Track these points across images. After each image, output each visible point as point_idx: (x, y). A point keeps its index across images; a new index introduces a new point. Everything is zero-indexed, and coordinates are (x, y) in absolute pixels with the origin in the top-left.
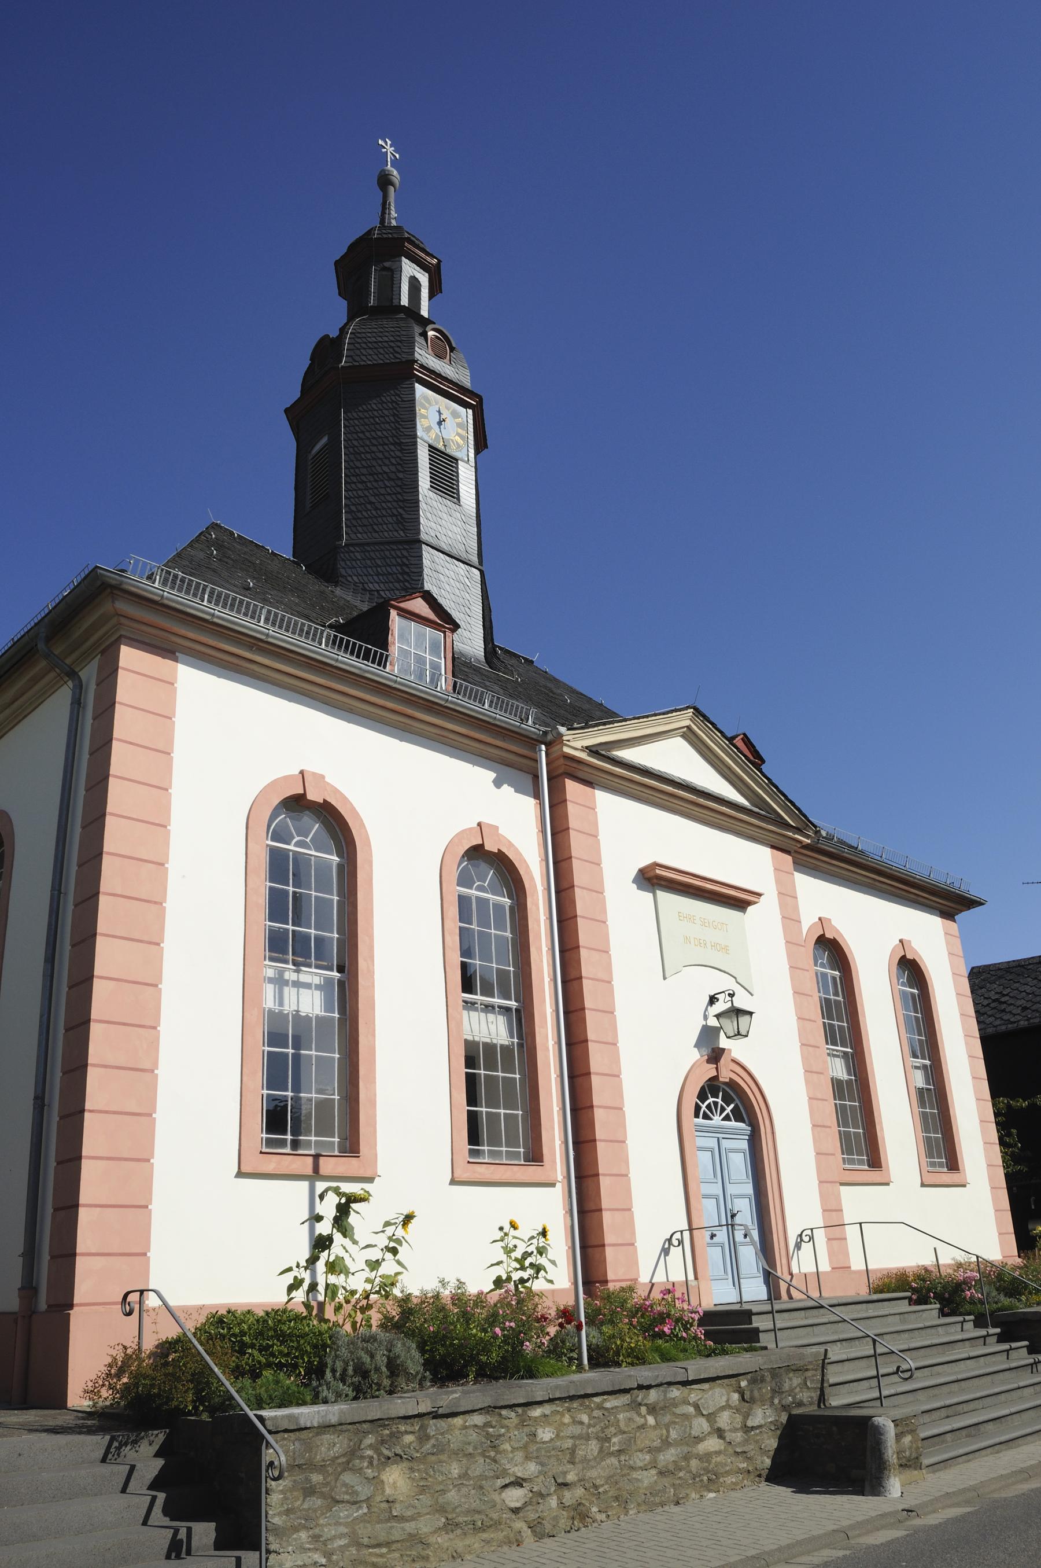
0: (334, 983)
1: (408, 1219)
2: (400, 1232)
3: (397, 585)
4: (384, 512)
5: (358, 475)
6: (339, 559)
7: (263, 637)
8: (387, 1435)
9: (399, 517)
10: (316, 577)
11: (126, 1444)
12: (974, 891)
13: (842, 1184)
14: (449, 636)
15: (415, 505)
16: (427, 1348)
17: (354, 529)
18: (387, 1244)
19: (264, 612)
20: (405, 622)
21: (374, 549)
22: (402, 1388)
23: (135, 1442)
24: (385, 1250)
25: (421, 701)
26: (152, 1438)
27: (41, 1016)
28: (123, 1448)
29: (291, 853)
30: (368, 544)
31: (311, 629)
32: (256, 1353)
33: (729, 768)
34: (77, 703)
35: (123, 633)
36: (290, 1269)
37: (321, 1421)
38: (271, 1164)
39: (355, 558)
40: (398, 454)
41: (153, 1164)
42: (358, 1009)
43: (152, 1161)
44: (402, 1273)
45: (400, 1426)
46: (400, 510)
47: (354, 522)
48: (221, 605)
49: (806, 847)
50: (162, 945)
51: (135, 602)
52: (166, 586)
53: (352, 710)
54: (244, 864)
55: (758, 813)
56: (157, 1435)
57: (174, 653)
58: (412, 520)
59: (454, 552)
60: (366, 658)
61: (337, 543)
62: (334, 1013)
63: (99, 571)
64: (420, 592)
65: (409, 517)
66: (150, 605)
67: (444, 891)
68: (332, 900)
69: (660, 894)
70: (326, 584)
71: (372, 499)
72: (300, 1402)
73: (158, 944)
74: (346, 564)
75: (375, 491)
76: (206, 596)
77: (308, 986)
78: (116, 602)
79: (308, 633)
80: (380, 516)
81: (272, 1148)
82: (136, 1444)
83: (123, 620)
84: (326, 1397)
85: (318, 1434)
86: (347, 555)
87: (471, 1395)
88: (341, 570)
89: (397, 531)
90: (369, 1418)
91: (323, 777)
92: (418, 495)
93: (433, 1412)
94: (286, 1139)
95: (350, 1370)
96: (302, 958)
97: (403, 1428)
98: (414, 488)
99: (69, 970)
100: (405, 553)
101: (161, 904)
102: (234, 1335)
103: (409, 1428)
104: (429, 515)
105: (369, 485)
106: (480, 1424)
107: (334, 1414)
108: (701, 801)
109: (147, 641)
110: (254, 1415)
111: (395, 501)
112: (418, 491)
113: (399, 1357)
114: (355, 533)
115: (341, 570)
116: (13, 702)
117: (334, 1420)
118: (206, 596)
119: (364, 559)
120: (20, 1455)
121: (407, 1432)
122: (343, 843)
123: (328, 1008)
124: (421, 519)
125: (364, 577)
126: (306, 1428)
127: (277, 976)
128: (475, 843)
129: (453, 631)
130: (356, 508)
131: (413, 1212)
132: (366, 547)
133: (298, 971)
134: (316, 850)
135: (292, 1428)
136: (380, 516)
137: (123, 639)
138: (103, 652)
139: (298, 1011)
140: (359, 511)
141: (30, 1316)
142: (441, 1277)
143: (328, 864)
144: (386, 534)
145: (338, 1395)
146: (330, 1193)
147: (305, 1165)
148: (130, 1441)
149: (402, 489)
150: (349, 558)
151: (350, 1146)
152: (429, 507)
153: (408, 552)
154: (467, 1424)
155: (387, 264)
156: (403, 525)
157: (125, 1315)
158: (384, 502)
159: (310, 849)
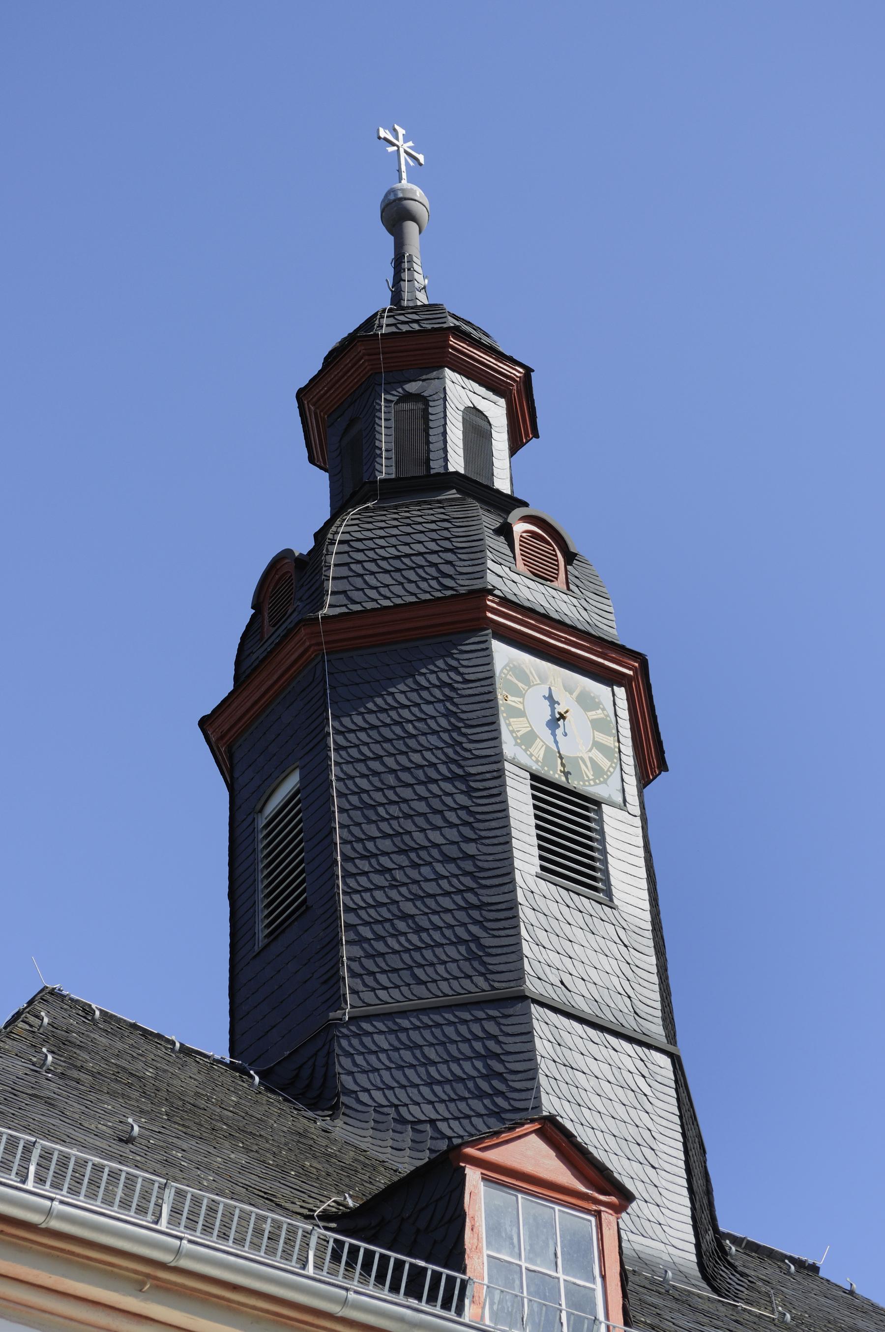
4: (437, 936)
5: (375, 855)
6: (337, 1050)
9: (473, 946)
10: (286, 1100)
14: (609, 1223)
17: (369, 980)
19: (169, 1196)
20: (501, 1196)
21: (418, 1023)
30: (403, 1013)
39: (374, 1048)
40: (463, 800)
46: (474, 929)
47: (369, 964)
52: (78, 1193)
58: (505, 950)
59: (607, 1017)
60: (414, 1291)
61: (332, 1015)
70: (310, 1114)
75: (415, 888)
76: (32, 1169)
80: (428, 946)
86: (355, 1042)
88: (343, 1077)
89: (469, 977)
92: (514, 891)
104: (542, 936)
105: (398, 875)
111: (461, 908)
114: (373, 990)
115: (343, 1077)
118: (32, 1169)
119: (397, 1050)
125: (397, 1090)
129: (619, 1209)
136: (428, 946)
144: (444, 985)
149: (475, 879)
153: (499, 1024)
155: (412, 387)
156: (484, 964)
158: (435, 912)
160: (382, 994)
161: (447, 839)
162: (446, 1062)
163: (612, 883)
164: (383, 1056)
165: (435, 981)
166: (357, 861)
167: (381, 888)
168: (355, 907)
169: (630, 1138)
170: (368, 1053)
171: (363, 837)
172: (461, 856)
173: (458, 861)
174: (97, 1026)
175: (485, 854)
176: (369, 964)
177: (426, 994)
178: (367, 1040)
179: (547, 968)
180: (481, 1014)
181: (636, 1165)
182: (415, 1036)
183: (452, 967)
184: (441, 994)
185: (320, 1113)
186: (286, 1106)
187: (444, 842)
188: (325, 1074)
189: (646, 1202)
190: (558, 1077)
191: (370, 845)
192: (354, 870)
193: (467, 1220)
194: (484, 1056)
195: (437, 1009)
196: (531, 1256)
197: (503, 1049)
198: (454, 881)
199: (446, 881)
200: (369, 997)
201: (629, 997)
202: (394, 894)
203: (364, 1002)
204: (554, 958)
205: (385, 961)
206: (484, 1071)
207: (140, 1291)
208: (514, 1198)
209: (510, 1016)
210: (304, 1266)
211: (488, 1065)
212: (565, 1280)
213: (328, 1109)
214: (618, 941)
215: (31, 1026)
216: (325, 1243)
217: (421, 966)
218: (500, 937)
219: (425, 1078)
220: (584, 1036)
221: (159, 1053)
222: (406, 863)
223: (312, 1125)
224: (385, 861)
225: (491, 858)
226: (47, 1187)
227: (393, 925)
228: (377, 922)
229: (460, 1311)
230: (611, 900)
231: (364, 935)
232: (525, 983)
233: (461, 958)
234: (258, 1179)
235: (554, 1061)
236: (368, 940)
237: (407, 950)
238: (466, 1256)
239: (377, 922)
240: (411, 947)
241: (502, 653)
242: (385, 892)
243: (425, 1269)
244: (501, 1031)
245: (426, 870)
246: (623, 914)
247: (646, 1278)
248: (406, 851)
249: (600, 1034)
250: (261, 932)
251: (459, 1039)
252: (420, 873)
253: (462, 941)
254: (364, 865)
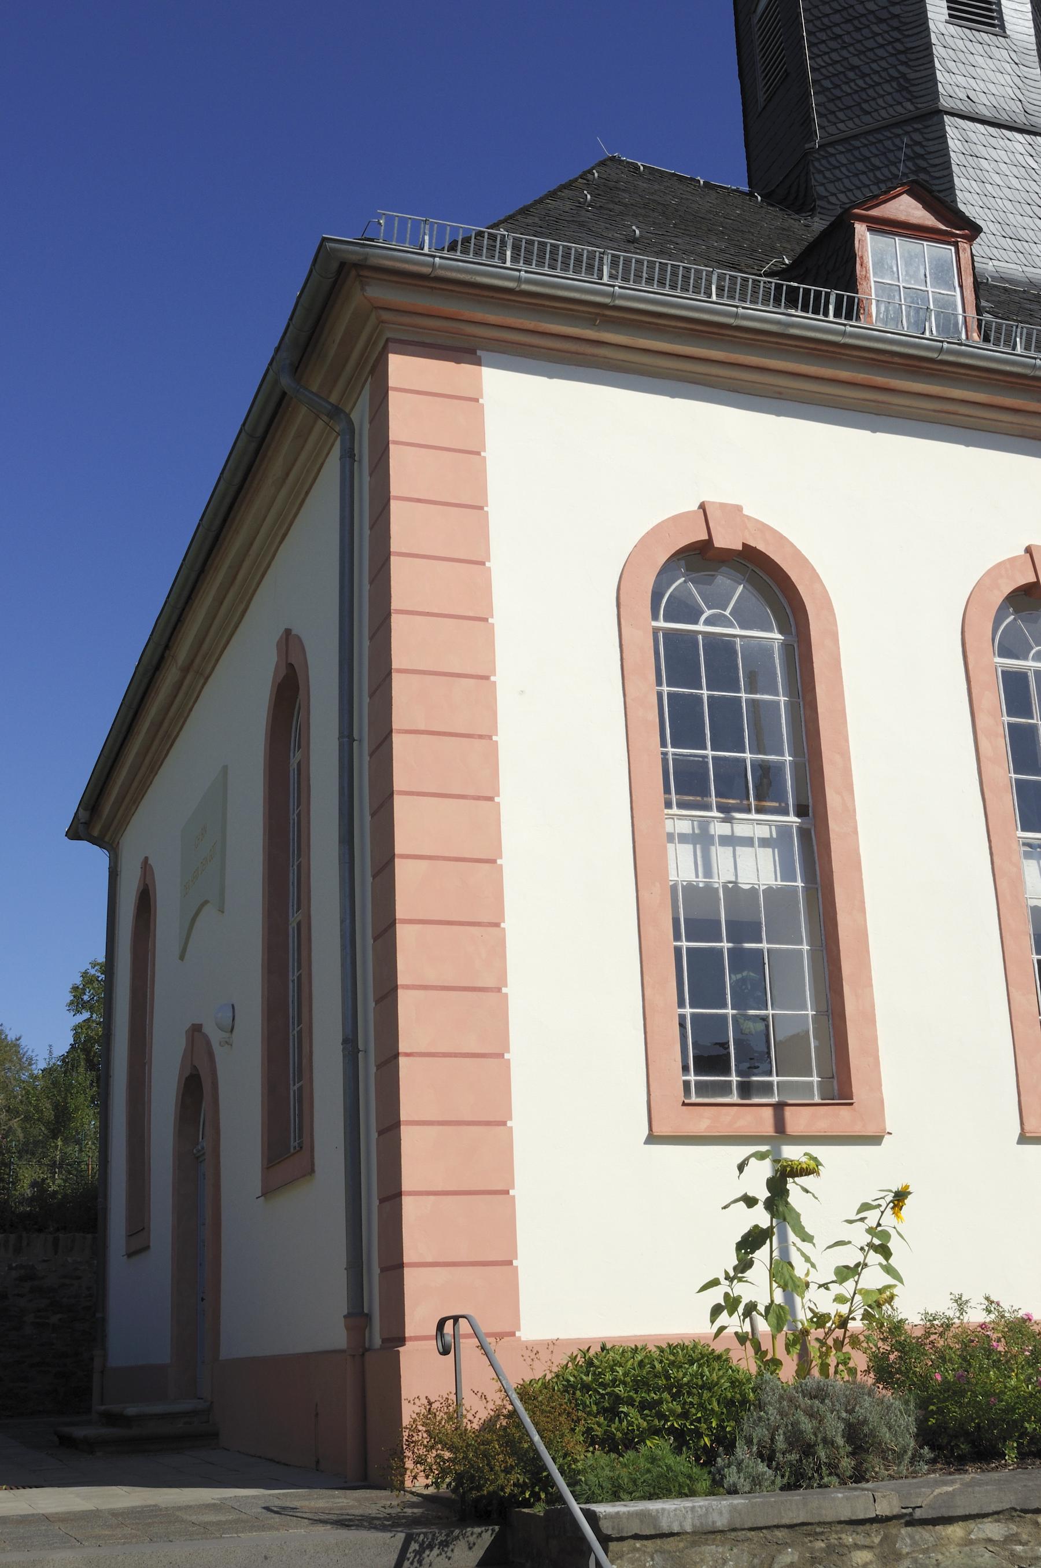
0: (792, 833)
1: (900, 1197)
2: (889, 1220)
4: (876, 78)
5: (829, 27)
6: (812, 170)
7: (607, 300)
8: (822, 1550)
9: (901, 81)
10: (781, 210)
11: (431, 1547)
14: (964, 249)
15: (925, 53)
16: (932, 1407)
17: (831, 117)
18: (869, 1241)
19: (607, 260)
20: (884, 241)
21: (866, 142)
22: (876, 1473)
23: (444, 1544)
24: (866, 1248)
25: (897, 360)
26: (472, 1539)
27: (342, 921)
28: (427, 1552)
29: (700, 637)
30: (855, 137)
31: (735, 284)
32: (633, 1412)
34: (349, 455)
35: (389, 335)
36: (715, 1283)
37: (698, 1525)
38: (703, 1121)
39: (837, 164)
41: (511, 1128)
42: (832, 872)
43: (509, 1124)
44: (895, 1286)
45: (843, 1536)
46: (902, 68)
47: (831, 106)
48: (534, 262)
50: (497, 799)
51: (397, 282)
52: (580, 272)
53: (780, 393)
54: (619, 663)
56: (480, 1534)
57: (473, 352)
58: (924, 80)
59: (1004, 117)
60: (792, 302)
61: (807, 146)
62: (796, 881)
63: (329, 245)
64: (902, 185)
65: (919, 75)
66: (443, 287)
67: (970, 667)
68: (778, 703)
70: (797, 217)
71: (855, 61)
72: (686, 1491)
73: (491, 799)
74: (825, 177)
75: (858, 46)
76: (509, 253)
77: (748, 842)
78: (367, 288)
79: (731, 290)
80: (871, 86)
81: (708, 1097)
82: (447, 1546)
83: (386, 316)
84: (735, 1485)
85: (694, 1544)
86: (824, 162)
87: (977, 1488)
88: (818, 188)
89: (900, 103)
90: (786, 1521)
91: (739, 508)
92: (929, 35)
93: (906, 1514)
94: (730, 1082)
95: (781, 1443)
96: (733, 799)
97: (849, 1540)
98: (921, 25)
99: (372, 852)
100: (917, 137)
101: (490, 737)
102: (604, 1385)
103: (861, 1540)
104: (951, 65)
105: (847, 39)
106: (996, 1537)
107: (721, 1513)
109: (428, 341)
110: (580, 1508)
111: (892, 55)
112: (928, 28)
113: (865, 1422)
114: (835, 124)
115: (818, 188)
116: (287, 475)
117: (721, 1522)
118: (509, 253)
119: (853, 163)
120: (266, 1558)
121: (857, 1547)
122: (788, 611)
123: (787, 873)
124: (938, 74)
125: (855, 191)
126: (672, 1534)
127: (697, 831)
128: (1022, 581)
129: (971, 239)
130: (831, 82)
131: (907, 1187)
132: (852, 142)
133: (728, 820)
134: (742, 627)
135: (647, 1532)
136: (871, 86)
137: (390, 344)
138: (372, 372)
139: (735, 883)
140: (837, 86)
141: (363, 1355)
142: (956, 1292)
143: (764, 650)
144: (883, 113)
145: (756, 1482)
146: (752, 1160)
147: (763, 1120)
148: (437, 1542)
150: (828, 166)
151: (839, 1090)
152: (950, 51)
153: (922, 133)
154: (973, 1537)
156: (910, 92)
157: (441, 1354)
158: (874, 61)
159: (732, 626)
160: (841, 126)
161: (879, 6)
162: (887, 166)
163: (1005, 19)
164: (843, 169)
165: (876, 110)
166: (817, 34)
167: (836, 50)
168: (818, 67)
169: (1023, 201)
170: (833, 169)
171: (820, 15)
172: (890, 16)
173: (888, 21)
174: (643, 177)
175: (907, 12)
176: (831, 106)
177: (871, 120)
178: (832, 160)
179: (956, 88)
180: (909, 129)
181: (1027, 219)
182: (865, 152)
183: (888, 98)
184: (881, 119)
185: (804, 215)
186: (780, 214)
187: (877, 8)
188: (806, 187)
189: (1036, 243)
190: (966, 164)
191: (826, 20)
192: (816, 41)
193: (857, 259)
194: (912, 158)
195: (877, 130)
196: (907, 278)
197: (925, 150)
198: (886, 36)
199: (880, 37)
200: (832, 129)
201: (1020, 101)
202: (844, 53)
203: (829, 134)
204: (961, 80)
205: (842, 102)
206: (913, 168)
207: (594, 325)
208: (893, 240)
209: (929, 126)
210: (710, 296)
211: (916, 164)
212: (932, 292)
213: (809, 212)
214: (1010, 61)
215: (588, 181)
216: (769, 290)
217: (866, 101)
218: (920, 71)
219: (873, 179)
220: (986, 133)
221: (688, 189)
222: (852, 29)
223: (797, 223)
224: (837, 30)
225: (911, 14)
226: (631, 283)
227: (845, 76)
228: (834, 75)
229: (858, 319)
230: (1005, 32)
231: (825, 86)
232: (939, 101)
233: (894, 90)
234: (731, 257)
235: (964, 154)
236: (828, 89)
237: (856, 92)
238: (858, 284)
239: (834, 75)
240: (859, 89)
242: (838, 53)
243: (799, 288)
244: (925, 138)
245: (866, 32)
246: (1014, 41)
247: (1034, 294)
248: (851, 20)
249: (998, 130)
250: (762, 98)
251: (894, 148)
252: (862, 35)
253: (893, 79)
254: (823, 36)
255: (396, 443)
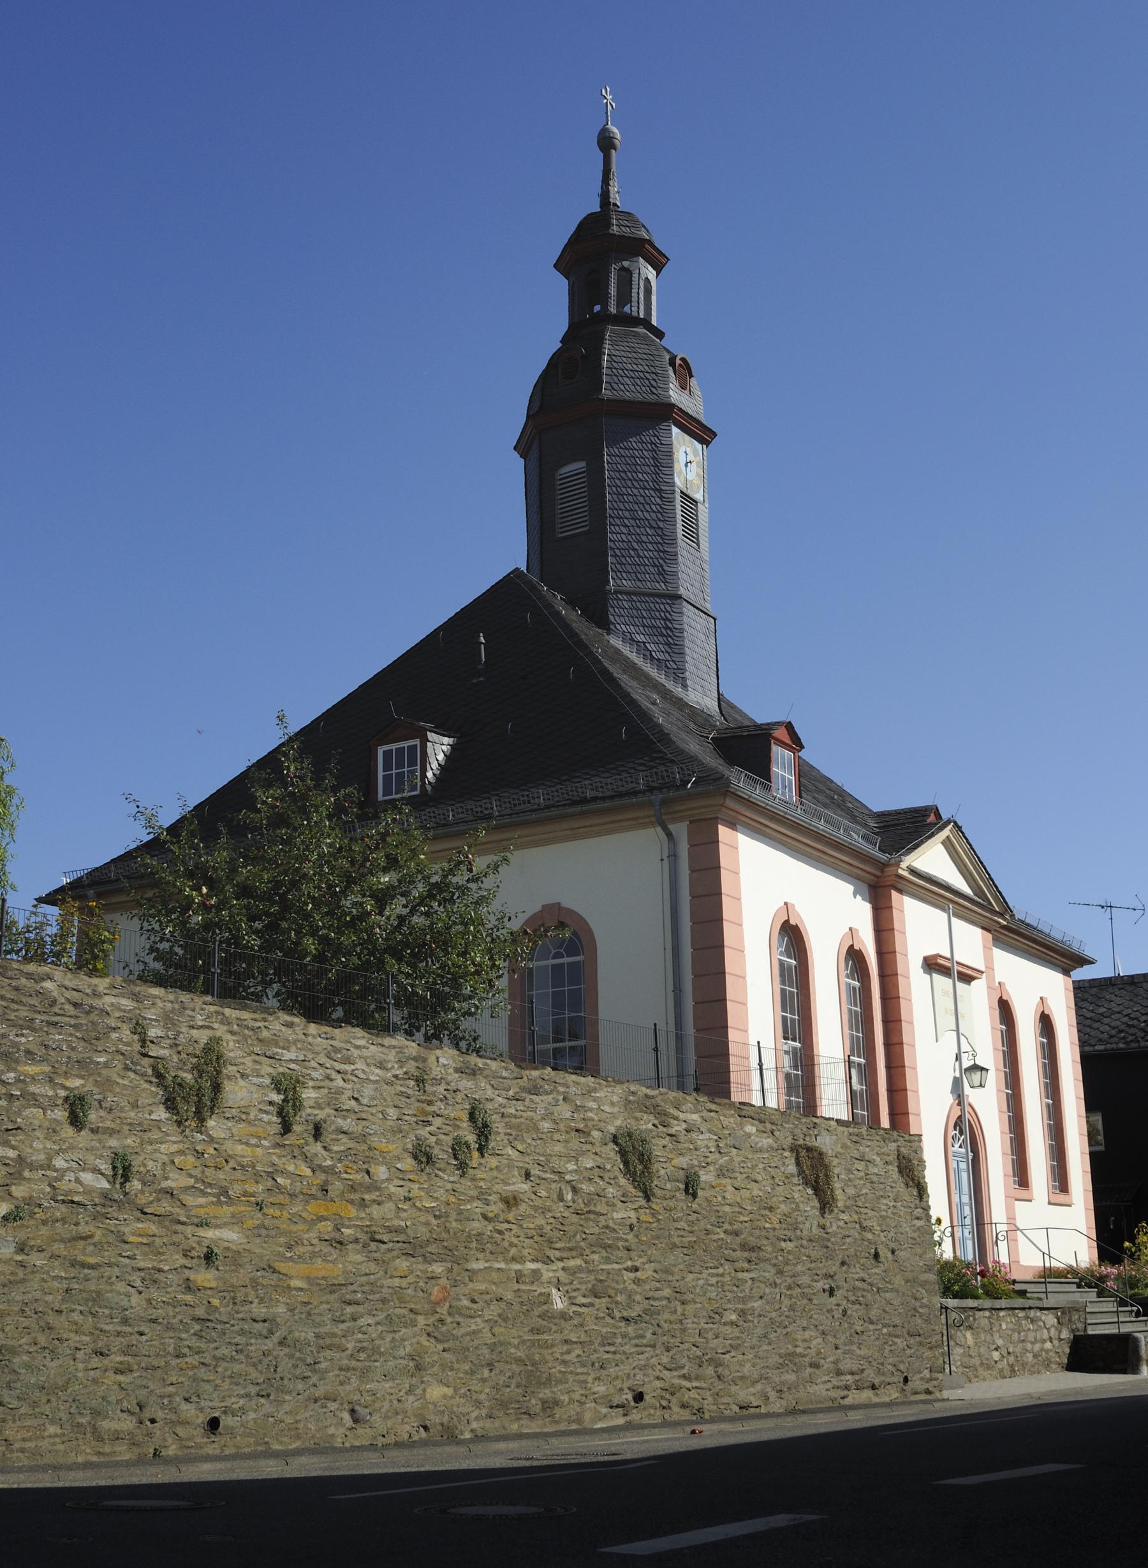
3: (660, 638)
12: (1088, 952)
13: (1016, 1200)
17: (619, 574)
30: (635, 594)
33: (966, 866)
40: (658, 500)
46: (661, 561)
49: (1004, 927)
55: (980, 903)
65: (669, 569)
69: (935, 975)
71: (635, 545)
108: (956, 899)
149: (662, 539)
155: (626, 264)
241: (675, 430)
255: (731, 1028)
